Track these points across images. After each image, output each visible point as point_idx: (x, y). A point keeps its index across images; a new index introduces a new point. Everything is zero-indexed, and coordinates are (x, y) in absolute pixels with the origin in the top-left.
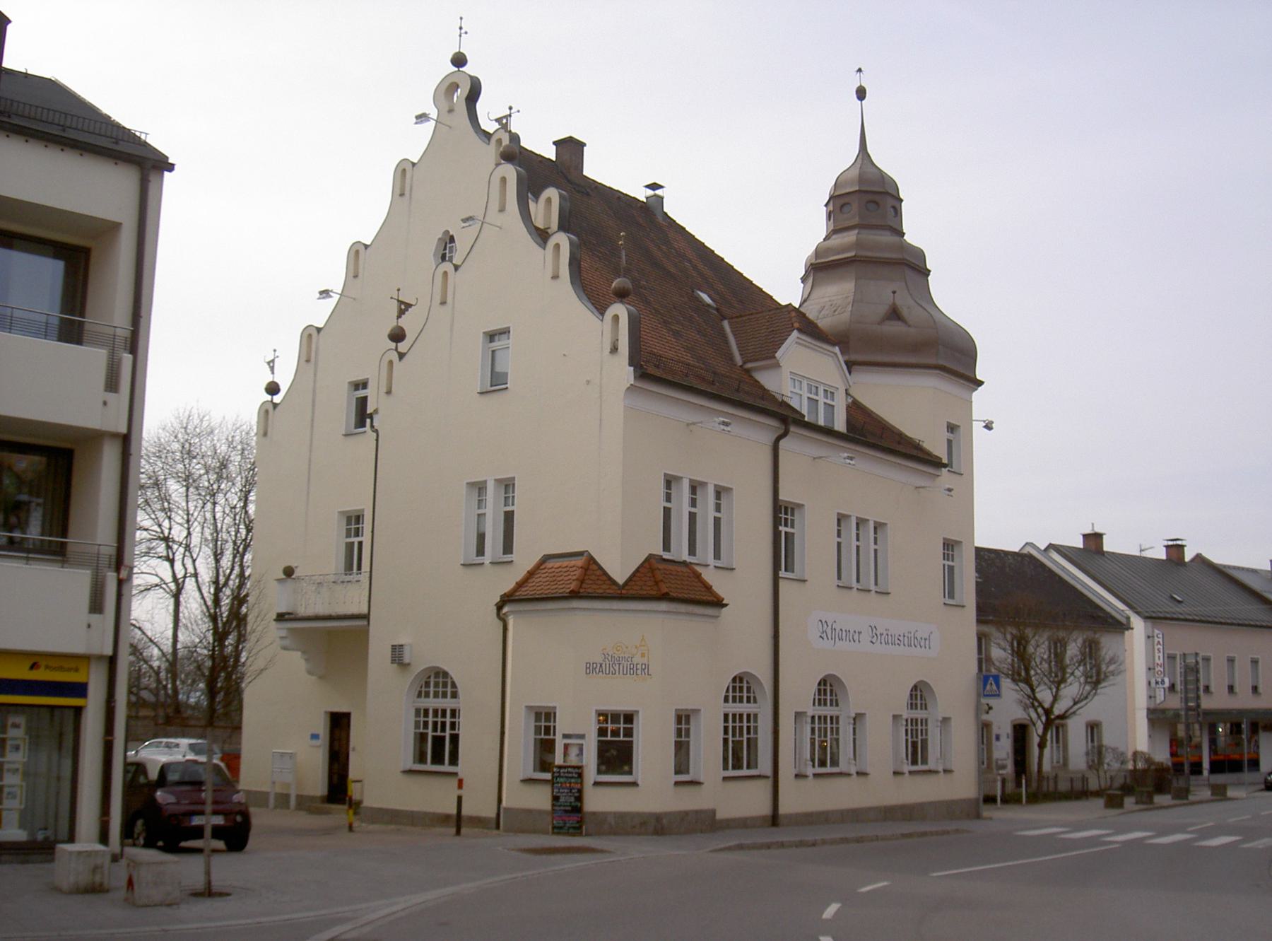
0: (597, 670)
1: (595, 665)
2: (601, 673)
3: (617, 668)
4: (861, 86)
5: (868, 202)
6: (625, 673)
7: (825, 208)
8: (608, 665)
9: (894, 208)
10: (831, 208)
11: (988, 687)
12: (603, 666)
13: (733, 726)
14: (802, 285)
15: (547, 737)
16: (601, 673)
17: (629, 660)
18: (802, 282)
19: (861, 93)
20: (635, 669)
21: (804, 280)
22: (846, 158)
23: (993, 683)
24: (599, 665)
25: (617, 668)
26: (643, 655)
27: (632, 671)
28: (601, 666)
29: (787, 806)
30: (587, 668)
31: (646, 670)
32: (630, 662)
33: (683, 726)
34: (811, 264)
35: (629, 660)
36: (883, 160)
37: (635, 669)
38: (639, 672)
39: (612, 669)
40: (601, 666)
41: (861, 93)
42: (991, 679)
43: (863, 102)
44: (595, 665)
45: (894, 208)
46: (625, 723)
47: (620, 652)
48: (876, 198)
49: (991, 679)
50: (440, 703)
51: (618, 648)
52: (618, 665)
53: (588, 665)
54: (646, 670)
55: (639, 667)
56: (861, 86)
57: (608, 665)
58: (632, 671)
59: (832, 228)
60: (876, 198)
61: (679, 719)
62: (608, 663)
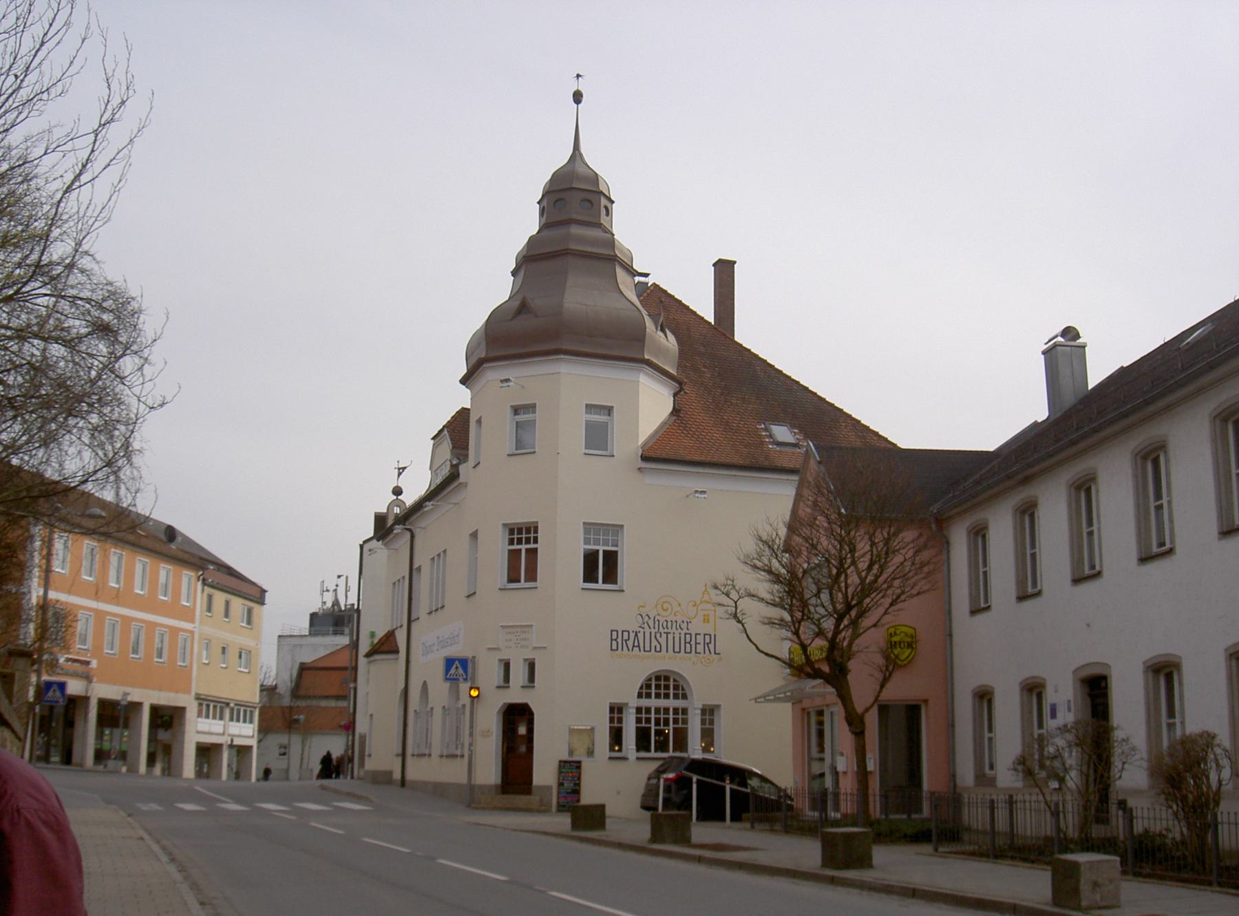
0: (630, 643)
1: (626, 634)
2: (636, 649)
3: (663, 640)
4: (578, 90)
5: (582, 201)
6: (677, 649)
7: (538, 205)
8: (647, 635)
9: (606, 208)
10: (545, 203)
11: (453, 671)
12: (640, 636)
13: (655, 718)
14: (513, 278)
15: (678, 754)
16: (636, 649)
17: (684, 626)
18: (513, 275)
19: (578, 97)
20: (693, 643)
21: (514, 273)
22: (561, 158)
23: (459, 665)
24: (632, 635)
25: (663, 640)
26: (706, 620)
27: (688, 640)
28: (636, 635)
29: (411, 775)
30: (612, 640)
31: (712, 646)
32: (685, 631)
33: (616, 715)
34: (524, 257)
35: (684, 626)
36: (594, 159)
37: (693, 643)
38: (700, 648)
39: (654, 643)
40: (636, 635)
41: (578, 97)
42: (457, 662)
43: (579, 106)
44: (626, 634)
45: (606, 208)
46: (642, 718)
47: (668, 613)
48: (589, 196)
49: (457, 662)
50: (671, 703)
51: (665, 606)
52: (664, 636)
53: (614, 633)
54: (712, 646)
55: (700, 639)
56: (578, 90)
57: (647, 635)
58: (688, 645)
59: (544, 221)
60: (589, 196)
61: (612, 710)
62: (647, 631)
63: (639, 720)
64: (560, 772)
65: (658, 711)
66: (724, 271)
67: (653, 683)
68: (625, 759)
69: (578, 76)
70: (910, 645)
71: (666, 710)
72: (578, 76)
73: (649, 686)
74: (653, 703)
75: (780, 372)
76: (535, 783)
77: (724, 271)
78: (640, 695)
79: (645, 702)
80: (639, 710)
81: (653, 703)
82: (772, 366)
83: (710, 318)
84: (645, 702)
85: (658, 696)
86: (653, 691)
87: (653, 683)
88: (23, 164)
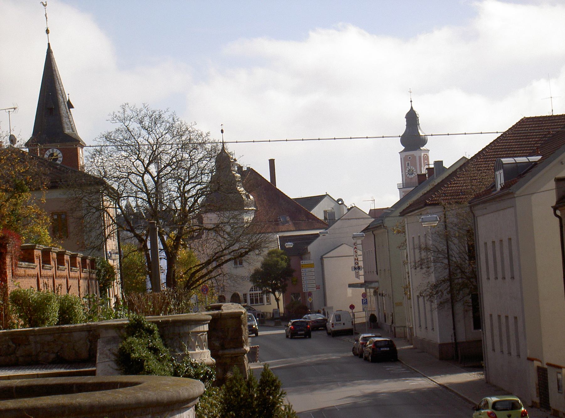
61: (244, 295)
63: (250, 297)
64: (538, 371)
65: (255, 294)
66: (272, 162)
67: (253, 288)
68: (264, 305)
69: (222, 125)
70: (296, 281)
71: (257, 294)
72: (222, 125)
73: (252, 288)
74: (254, 292)
75: (287, 196)
76: (259, 335)
77: (272, 162)
78: (250, 291)
79: (251, 292)
80: (250, 294)
81: (254, 292)
82: (284, 194)
83: (269, 181)
84: (251, 292)
85: (255, 290)
86: (253, 290)
87: (253, 288)
88: (187, 271)
